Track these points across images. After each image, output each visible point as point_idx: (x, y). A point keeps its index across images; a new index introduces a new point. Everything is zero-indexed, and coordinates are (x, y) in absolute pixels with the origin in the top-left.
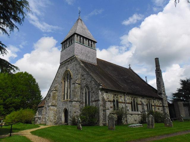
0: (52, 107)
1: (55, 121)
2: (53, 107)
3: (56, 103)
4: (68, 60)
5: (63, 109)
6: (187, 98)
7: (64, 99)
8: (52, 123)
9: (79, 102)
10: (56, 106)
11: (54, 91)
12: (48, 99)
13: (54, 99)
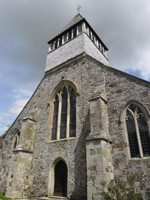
0: (23, 155)
1: (27, 186)
2: (25, 154)
3: (32, 147)
4: (67, 64)
5: (53, 159)
6: (148, 148)
7: (54, 137)
8: (20, 194)
9: (111, 143)
10: (32, 153)
11: (31, 121)
12: (11, 139)
13: (29, 138)
